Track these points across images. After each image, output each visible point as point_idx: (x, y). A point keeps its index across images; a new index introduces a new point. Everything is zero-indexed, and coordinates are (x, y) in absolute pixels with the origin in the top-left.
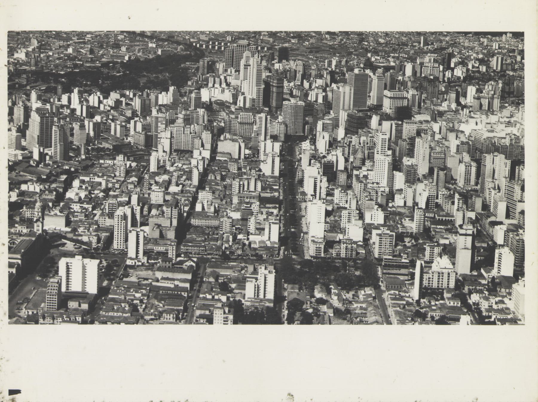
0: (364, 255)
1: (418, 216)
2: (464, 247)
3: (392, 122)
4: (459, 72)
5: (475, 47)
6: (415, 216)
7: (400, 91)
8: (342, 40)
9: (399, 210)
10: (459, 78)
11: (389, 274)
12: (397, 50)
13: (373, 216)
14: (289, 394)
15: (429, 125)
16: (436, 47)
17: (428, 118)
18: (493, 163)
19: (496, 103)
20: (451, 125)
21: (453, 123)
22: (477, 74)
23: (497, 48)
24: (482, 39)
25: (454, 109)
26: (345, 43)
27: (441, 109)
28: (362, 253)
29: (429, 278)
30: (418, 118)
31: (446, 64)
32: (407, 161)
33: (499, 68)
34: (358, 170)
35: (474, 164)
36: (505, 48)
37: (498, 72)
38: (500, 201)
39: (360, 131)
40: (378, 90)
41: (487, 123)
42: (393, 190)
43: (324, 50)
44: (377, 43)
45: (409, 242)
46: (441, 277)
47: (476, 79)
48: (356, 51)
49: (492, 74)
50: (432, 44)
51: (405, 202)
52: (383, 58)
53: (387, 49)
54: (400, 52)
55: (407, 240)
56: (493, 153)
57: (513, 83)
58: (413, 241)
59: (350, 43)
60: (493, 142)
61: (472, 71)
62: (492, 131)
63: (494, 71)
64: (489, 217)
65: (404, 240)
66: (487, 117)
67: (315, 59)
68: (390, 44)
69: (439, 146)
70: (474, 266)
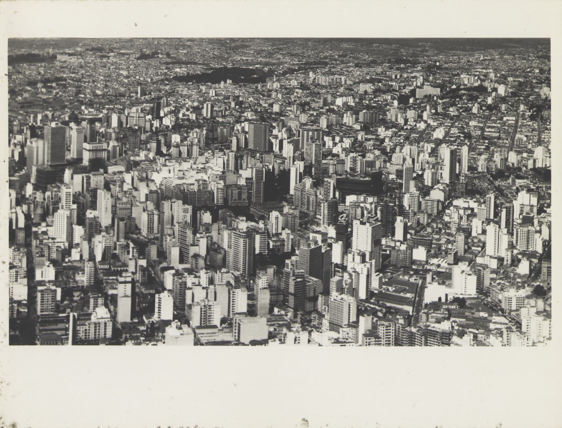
0: (26, 314)
1: (89, 269)
2: (123, 295)
3: (84, 175)
4: (168, 121)
5: (192, 95)
6: (86, 269)
7: (99, 143)
8: (57, 93)
9: (75, 264)
10: (167, 127)
11: (45, 330)
12: (113, 102)
13: (44, 272)
14: (304, 420)
15: (121, 176)
16: (153, 97)
17: (122, 169)
18: (171, 210)
19: (195, 149)
20: (144, 175)
21: (146, 172)
22: (186, 122)
23: (214, 95)
24: (201, 87)
25: (152, 158)
26: (61, 96)
27: (138, 159)
28: (25, 312)
29: (86, 330)
30: (111, 169)
31: (155, 114)
32: (90, 214)
33: (209, 115)
34: (36, 227)
35: (156, 212)
36: (221, 94)
37: (208, 119)
38: (173, 246)
39: (49, 186)
40: (77, 143)
41: (180, 171)
42: (72, 244)
43: (37, 105)
44: (93, 96)
45: (78, 296)
46: (98, 328)
47: (185, 127)
48: (70, 104)
49: (202, 121)
50: (150, 94)
51: (81, 256)
52: (97, 110)
53: (103, 101)
54: (116, 104)
55: (76, 294)
56: (171, 200)
57: (217, 130)
58: (82, 295)
59: (65, 97)
60: (182, 189)
61: (182, 119)
62: (182, 178)
63: (204, 118)
64: (161, 263)
65: (73, 294)
66: (180, 163)
67: (25, 114)
68: (107, 95)
69: (126, 197)
70: (134, 314)
